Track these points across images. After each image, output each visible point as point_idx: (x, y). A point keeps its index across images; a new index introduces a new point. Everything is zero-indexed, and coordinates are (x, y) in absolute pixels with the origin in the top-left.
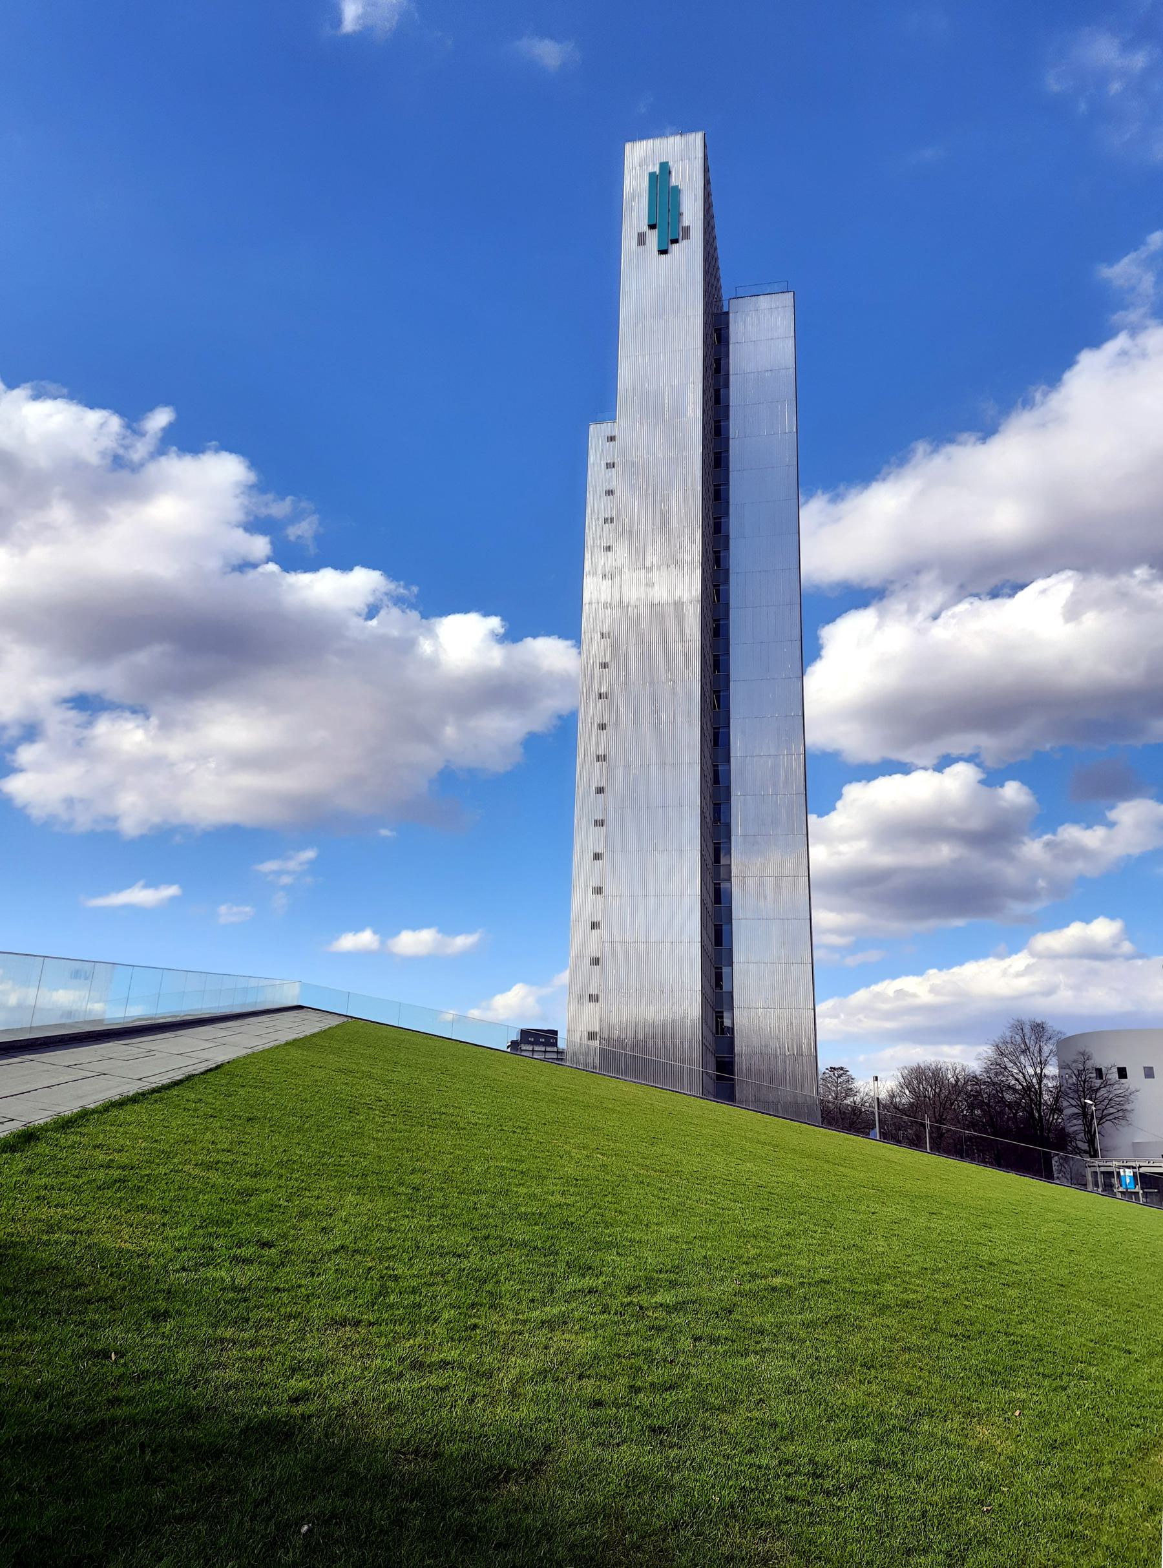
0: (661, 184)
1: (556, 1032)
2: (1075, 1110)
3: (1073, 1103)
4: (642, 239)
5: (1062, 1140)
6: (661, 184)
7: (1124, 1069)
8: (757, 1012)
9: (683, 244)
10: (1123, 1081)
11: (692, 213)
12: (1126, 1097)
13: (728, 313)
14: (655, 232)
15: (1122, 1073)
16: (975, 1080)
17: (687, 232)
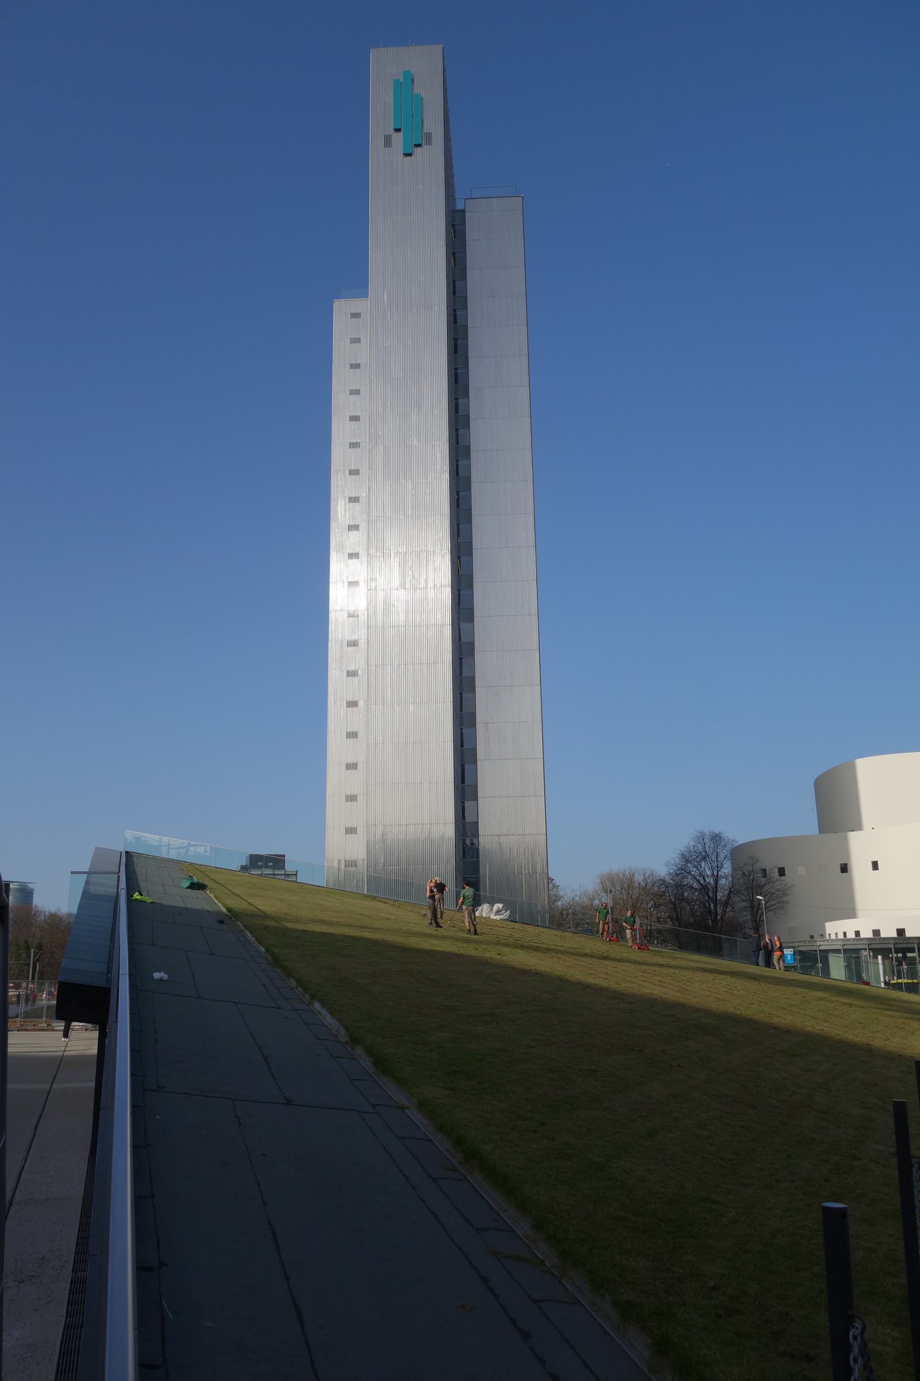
0: (405, 87)
1: (284, 856)
2: (745, 904)
3: (744, 898)
4: (388, 142)
5: (733, 928)
6: (405, 87)
7: (783, 869)
8: (497, 828)
9: (425, 148)
10: (783, 878)
11: (434, 124)
12: (785, 892)
13: (463, 211)
14: (401, 134)
15: (782, 872)
16: (663, 882)
17: (429, 138)
